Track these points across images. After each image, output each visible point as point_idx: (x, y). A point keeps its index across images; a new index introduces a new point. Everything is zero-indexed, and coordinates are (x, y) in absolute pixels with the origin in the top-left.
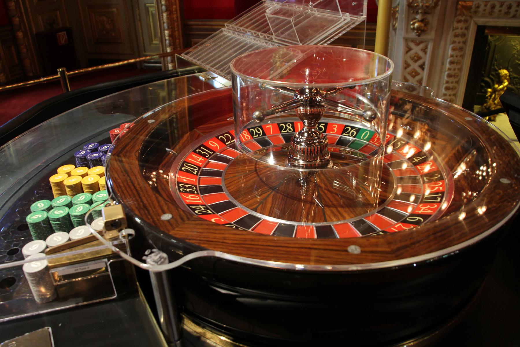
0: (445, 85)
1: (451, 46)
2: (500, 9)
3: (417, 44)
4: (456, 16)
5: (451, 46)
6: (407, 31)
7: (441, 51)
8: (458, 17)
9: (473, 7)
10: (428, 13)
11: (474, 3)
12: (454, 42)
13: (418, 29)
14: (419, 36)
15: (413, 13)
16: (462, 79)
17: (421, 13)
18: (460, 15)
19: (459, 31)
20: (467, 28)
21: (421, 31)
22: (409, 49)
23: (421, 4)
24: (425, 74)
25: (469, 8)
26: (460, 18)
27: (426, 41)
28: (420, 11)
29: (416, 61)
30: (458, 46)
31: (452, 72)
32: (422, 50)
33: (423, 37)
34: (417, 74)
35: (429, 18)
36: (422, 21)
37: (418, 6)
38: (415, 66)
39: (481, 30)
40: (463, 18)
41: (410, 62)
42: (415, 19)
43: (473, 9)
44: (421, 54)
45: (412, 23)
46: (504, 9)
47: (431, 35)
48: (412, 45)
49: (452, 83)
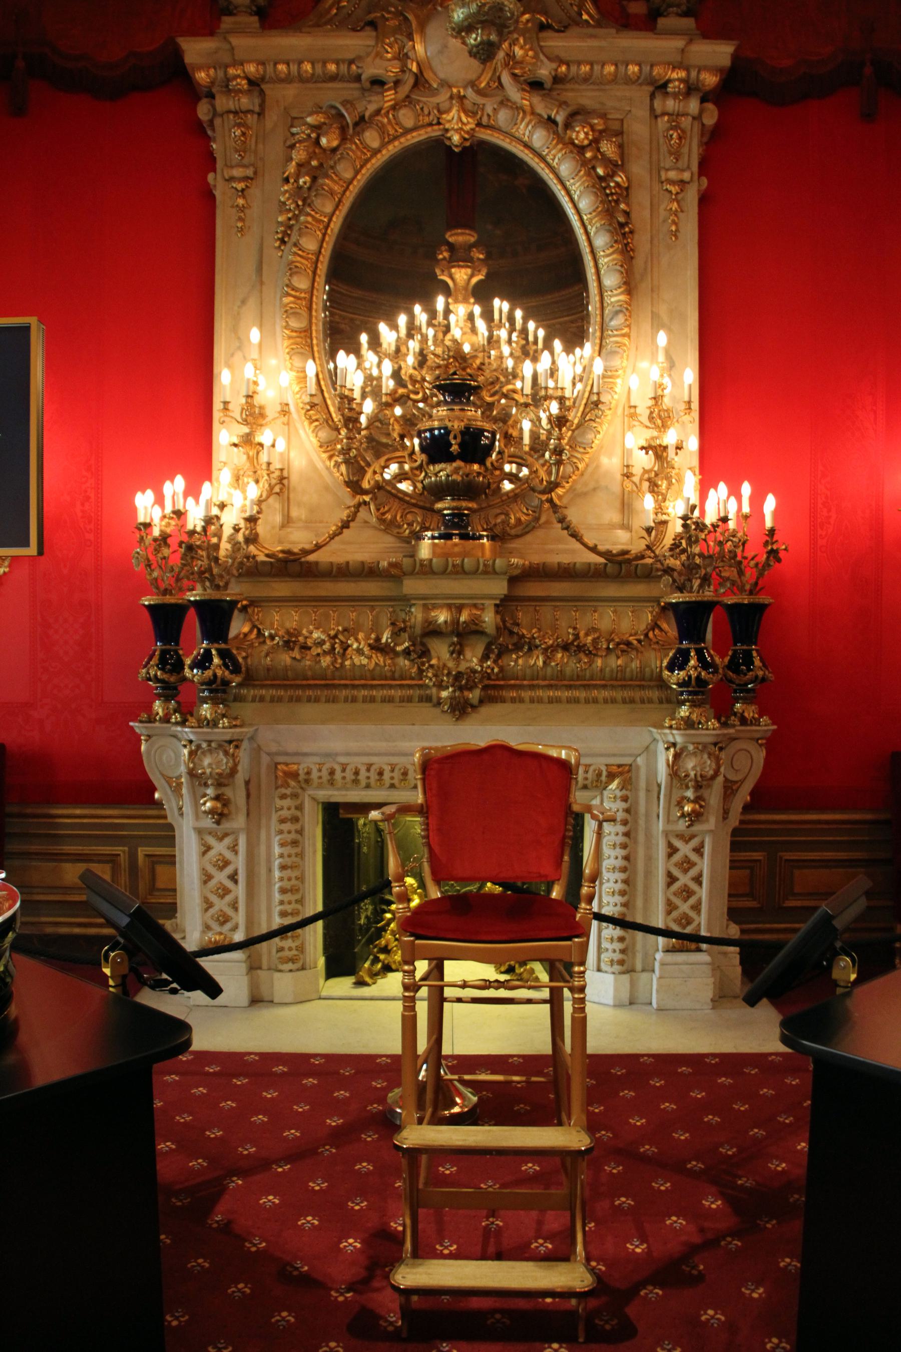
0: (279, 908)
1: (278, 838)
2: (343, 774)
3: (687, 842)
4: (277, 788)
5: (278, 838)
6: (197, 817)
7: (263, 848)
8: (279, 790)
9: (301, 772)
10: (225, 785)
11: (301, 767)
12: (281, 832)
13: (212, 812)
14: (218, 823)
15: (200, 785)
16: (307, 894)
17: (212, 785)
18: (282, 786)
19: (285, 813)
20: (300, 808)
21: (696, 817)
22: (208, 848)
23: (208, 771)
24: (240, 891)
25: (295, 775)
26: (283, 791)
27: (233, 833)
28: (209, 782)
29: (221, 868)
30: (289, 837)
31: (287, 885)
32: (228, 848)
33: (226, 825)
34: (227, 891)
35: (228, 792)
36: (217, 798)
37: (204, 773)
38: (221, 877)
39: (331, 810)
40: (288, 791)
41: (212, 870)
42: (205, 795)
43: (302, 777)
44: (229, 855)
45: (202, 801)
46: (349, 775)
47: (239, 821)
48: (211, 841)
49: (290, 903)
